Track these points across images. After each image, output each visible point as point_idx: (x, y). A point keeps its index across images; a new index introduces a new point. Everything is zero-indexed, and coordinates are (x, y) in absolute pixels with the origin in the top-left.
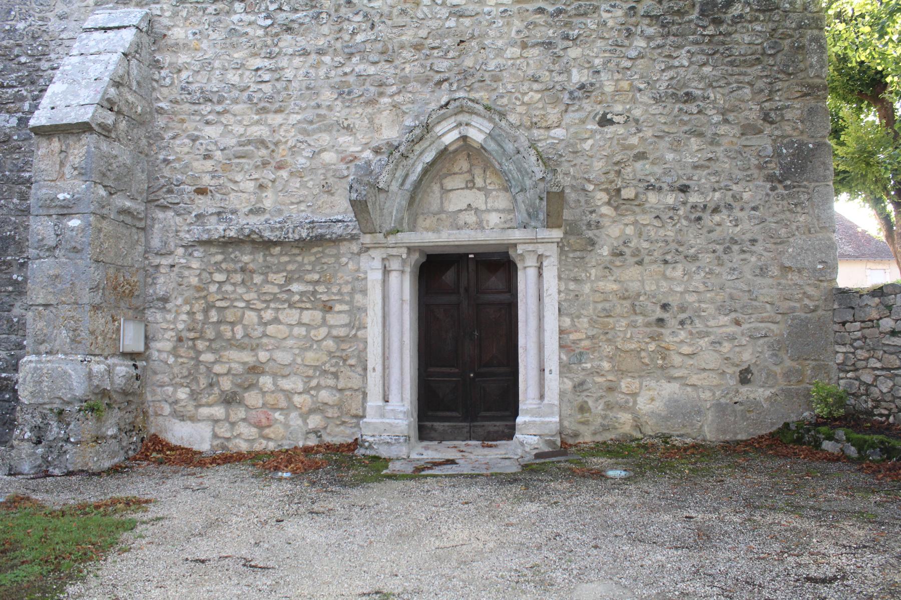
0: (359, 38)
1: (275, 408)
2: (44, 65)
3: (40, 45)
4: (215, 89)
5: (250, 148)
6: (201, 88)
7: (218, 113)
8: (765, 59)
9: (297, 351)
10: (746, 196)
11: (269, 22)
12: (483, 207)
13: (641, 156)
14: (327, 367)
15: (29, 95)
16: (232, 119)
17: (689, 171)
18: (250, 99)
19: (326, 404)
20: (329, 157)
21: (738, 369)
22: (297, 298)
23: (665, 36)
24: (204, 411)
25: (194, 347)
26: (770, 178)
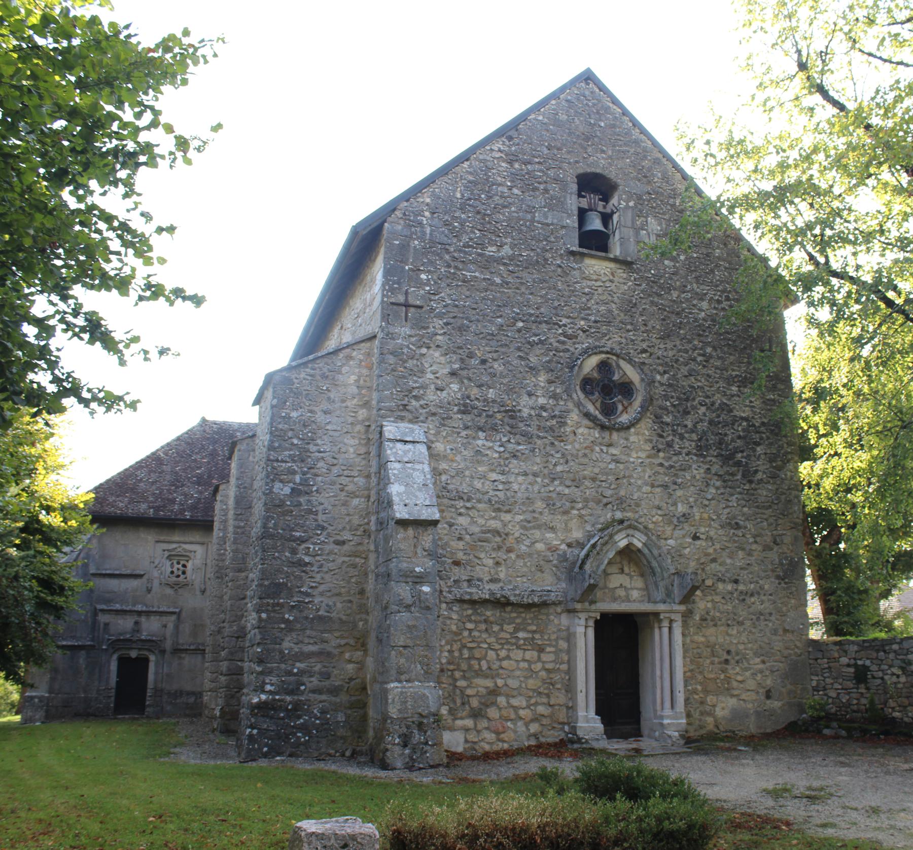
2: (312, 448)
5: (489, 535)
7: (467, 508)
9: (522, 679)
10: (766, 587)
11: (502, 449)
13: (714, 560)
14: (541, 690)
19: (543, 715)
20: (540, 546)
22: (522, 642)
23: (725, 487)
24: (459, 723)
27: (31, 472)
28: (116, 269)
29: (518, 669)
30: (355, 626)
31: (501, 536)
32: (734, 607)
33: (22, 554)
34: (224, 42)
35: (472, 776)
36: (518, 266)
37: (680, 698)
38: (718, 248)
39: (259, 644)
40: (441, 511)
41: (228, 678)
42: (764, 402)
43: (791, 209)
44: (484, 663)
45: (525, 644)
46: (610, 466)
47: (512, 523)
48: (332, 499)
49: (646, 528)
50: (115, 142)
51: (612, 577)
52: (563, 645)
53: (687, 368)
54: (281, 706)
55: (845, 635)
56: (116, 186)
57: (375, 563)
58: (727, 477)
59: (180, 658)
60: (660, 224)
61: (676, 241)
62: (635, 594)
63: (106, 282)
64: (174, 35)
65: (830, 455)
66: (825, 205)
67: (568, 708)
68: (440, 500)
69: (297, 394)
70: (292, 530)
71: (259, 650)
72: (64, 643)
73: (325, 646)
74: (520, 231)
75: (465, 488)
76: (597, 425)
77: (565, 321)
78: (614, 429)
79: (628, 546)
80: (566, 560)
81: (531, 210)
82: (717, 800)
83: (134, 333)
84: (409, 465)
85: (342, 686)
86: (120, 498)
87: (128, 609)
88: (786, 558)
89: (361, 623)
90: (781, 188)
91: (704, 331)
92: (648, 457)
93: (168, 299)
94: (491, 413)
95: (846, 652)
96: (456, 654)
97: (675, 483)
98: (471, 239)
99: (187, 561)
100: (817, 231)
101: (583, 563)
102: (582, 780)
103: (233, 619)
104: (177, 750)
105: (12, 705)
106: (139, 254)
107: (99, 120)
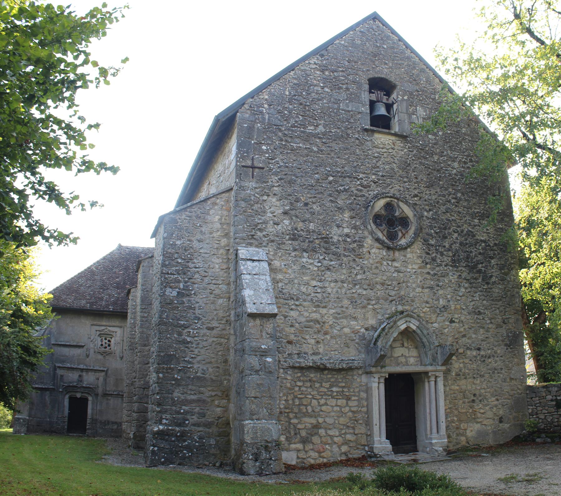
0: (359, 277)
2: (191, 265)
4: (295, 294)
5: (312, 323)
7: (297, 305)
9: (336, 418)
10: (498, 352)
11: (320, 264)
12: (408, 355)
13: (464, 336)
14: (349, 424)
15: (182, 280)
17: (480, 342)
18: (312, 300)
19: (350, 441)
20: (346, 330)
22: (335, 394)
23: (471, 288)
24: (293, 446)
27: (17, 280)
28: (65, 153)
29: (333, 411)
30: (222, 383)
31: (320, 324)
32: (478, 366)
33: (12, 330)
34: (128, 8)
35: (302, 480)
36: (329, 139)
37: (443, 426)
38: (464, 127)
39: (158, 393)
40: (279, 307)
41: (138, 414)
42: (495, 230)
43: (511, 104)
44: (309, 408)
45: (337, 395)
46: (394, 275)
47: (327, 315)
48: (205, 299)
49: (418, 316)
50: (63, 75)
51: (396, 350)
52: (363, 395)
53: (445, 207)
54: (172, 434)
55: (549, 381)
56: (63, 102)
57: (235, 342)
58: (472, 281)
59: (108, 399)
60: (425, 111)
61: (436, 123)
62: (412, 360)
63: (58, 162)
64: (97, 8)
65: (538, 264)
66: (532, 102)
67: (367, 435)
68: (277, 300)
69: (180, 229)
70: (179, 320)
71: (158, 397)
72: (37, 386)
73: (201, 396)
74: (330, 116)
75: (295, 292)
76: (385, 247)
77: (361, 176)
78: (396, 249)
79: (407, 329)
80: (365, 339)
81: (337, 102)
82: (468, 488)
83: (75, 194)
84: (256, 276)
85: (213, 421)
86: (69, 297)
87: (75, 367)
88: (511, 332)
89: (225, 382)
90: (504, 90)
91: (456, 182)
92: (420, 268)
93: (96, 170)
94: (311, 240)
95: (550, 392)
96: (290, 402)
97: (438, 286)
98: (296, 122)
99: (111, 338)
100: (528, 118)
101: (376, 340)
102: (377, 481)
103: (141, 376)
104: (106, 457)
105: (8, 422)
106: (78, 143)
107: (53, 63)
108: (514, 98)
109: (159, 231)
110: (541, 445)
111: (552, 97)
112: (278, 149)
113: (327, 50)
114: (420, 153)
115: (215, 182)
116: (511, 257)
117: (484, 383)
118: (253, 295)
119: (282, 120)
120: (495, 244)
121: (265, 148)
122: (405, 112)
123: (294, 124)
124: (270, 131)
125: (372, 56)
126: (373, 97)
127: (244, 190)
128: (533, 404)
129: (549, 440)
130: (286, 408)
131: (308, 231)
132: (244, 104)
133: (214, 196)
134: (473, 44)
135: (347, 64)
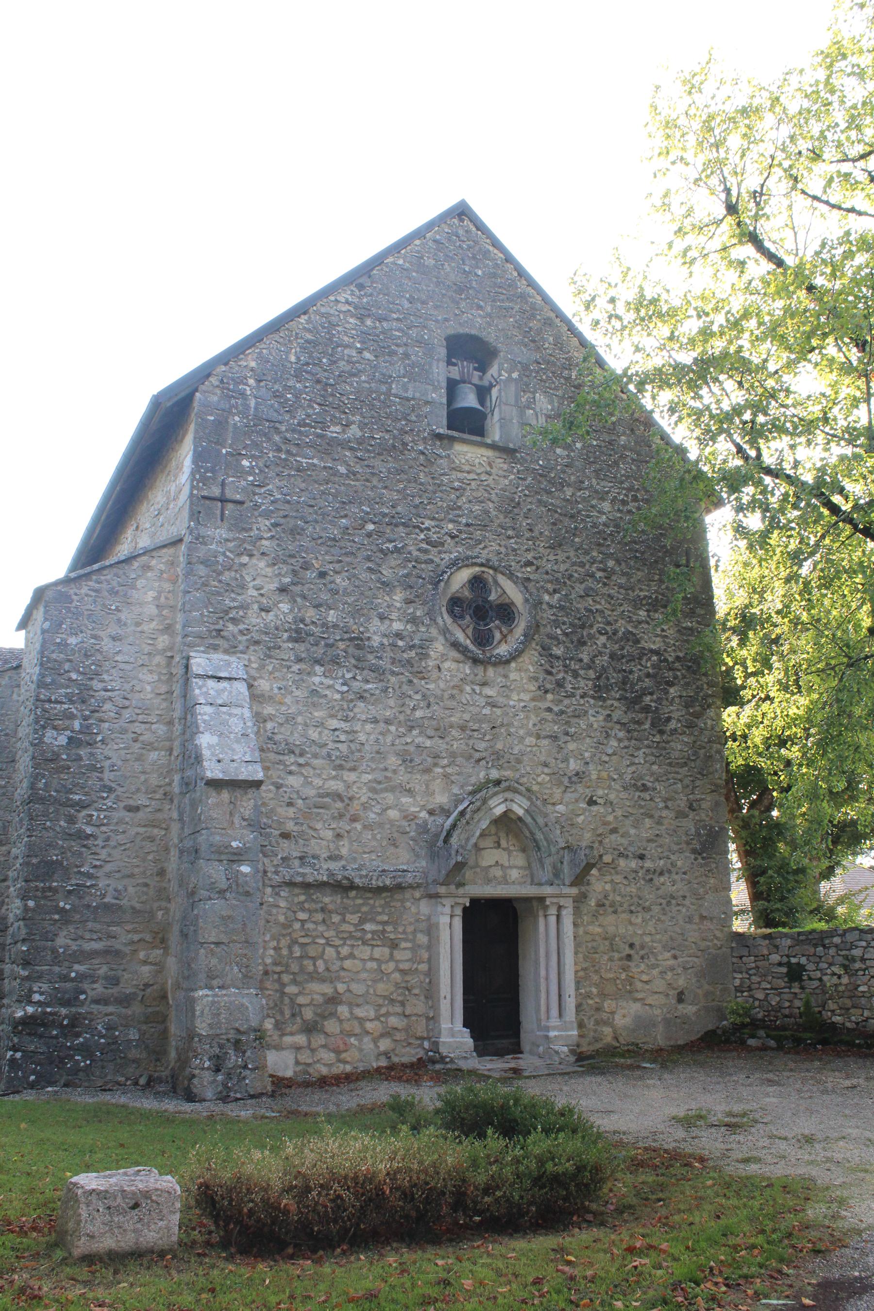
0: (419, 714)
1: (351, 1035)
2: (96, 684)
3: (92, 664)
4: (298, 743)
5: (327, 800)
6: (286, 740)
7: (300, 765)
8: (689, 762)
9: (370, 983)
10: (679, 863)
11: (345, 688)
12: (507, 864)
13: (614, 831)
14: (394, 996)
15: (79, 714)
16: (312, 772)
17: (645, 844)
18: (329, 755)
19: (396, 1029)
20: (393, 814)
21: (676, 992)
22: (369, 936)
23: (629, 739)
24: (288, 1039)
25: (279, 980)
26: (694, 851)
29: (364, 969)
30: (152, 914)
35: (304, 1108)
37: (570, 1003)
38: (624, 434)
39: (24, 940)
40: (266, 769)
42: (679, 631)
43: (715, 388)
46: (484, 711)
48: (123, 752)
49: (528, 790)
51: (485, 853)
52: (422, 939)
53: (583, 586)
55: (776, 926)
58: (632, 727)
60: (551, 402)
61: (571, 425)
65: (760, 698)
66: (756, 384)
67: (428, 1019)
68: (264, 755)
71: (24, 948)
74: (372, 407)
76: (470, 658)
77: (428, 523)
80: (427, 831)
81: (386, 380)
82: (615, 1132)
84: (224, 709)
85: (135, 993)
88: (704, 827)
89: (160, 913)
90: (702, 360)
91: (605, 539)
92: (533, 699)
94: (331, 641)
95: (777, 947)
97: (567, 734)
98: (308, 416)
100: (747, 416)
108: (722, 377)
109: (34, 617)
110: (757, 1053)
111: (796, 374)
112: (272, 467)
113: (370, 277)
114: (539, 482)
115: (148, 525)
116: (708, 684)
117: (651, 923)
118: (217, 745)
119: (282, 411)
120: (678, 658)
121: (248, 464)
122: (513, 403)
123: (304, 420)
124: (257, 432)
125: (455, 291)
126: (455, 373)
127: (206, 544)
128: (744, 969)
129: (772, 1043)
130: (275, 964)
131: (324, 625)
132: (209, 375)
133: (146, 552)
134: (646, 269)
135: (407, 305)
